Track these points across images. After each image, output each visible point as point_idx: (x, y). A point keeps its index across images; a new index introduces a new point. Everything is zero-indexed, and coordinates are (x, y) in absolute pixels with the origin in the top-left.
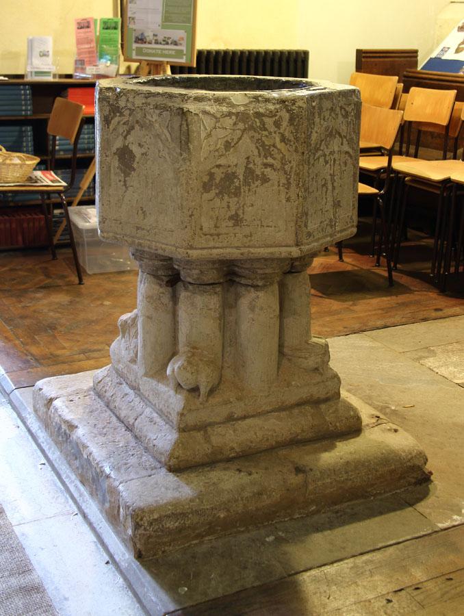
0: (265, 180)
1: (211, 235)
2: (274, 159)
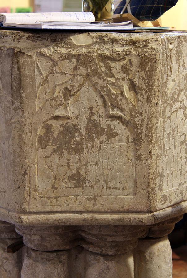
0: (111, 134)
1: (49, 198)
2: (122, 110)
